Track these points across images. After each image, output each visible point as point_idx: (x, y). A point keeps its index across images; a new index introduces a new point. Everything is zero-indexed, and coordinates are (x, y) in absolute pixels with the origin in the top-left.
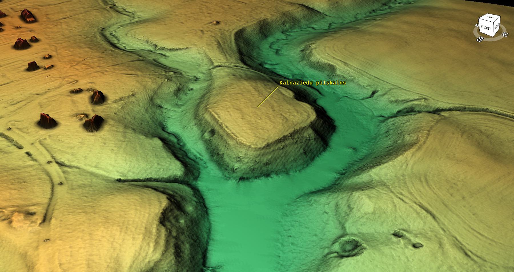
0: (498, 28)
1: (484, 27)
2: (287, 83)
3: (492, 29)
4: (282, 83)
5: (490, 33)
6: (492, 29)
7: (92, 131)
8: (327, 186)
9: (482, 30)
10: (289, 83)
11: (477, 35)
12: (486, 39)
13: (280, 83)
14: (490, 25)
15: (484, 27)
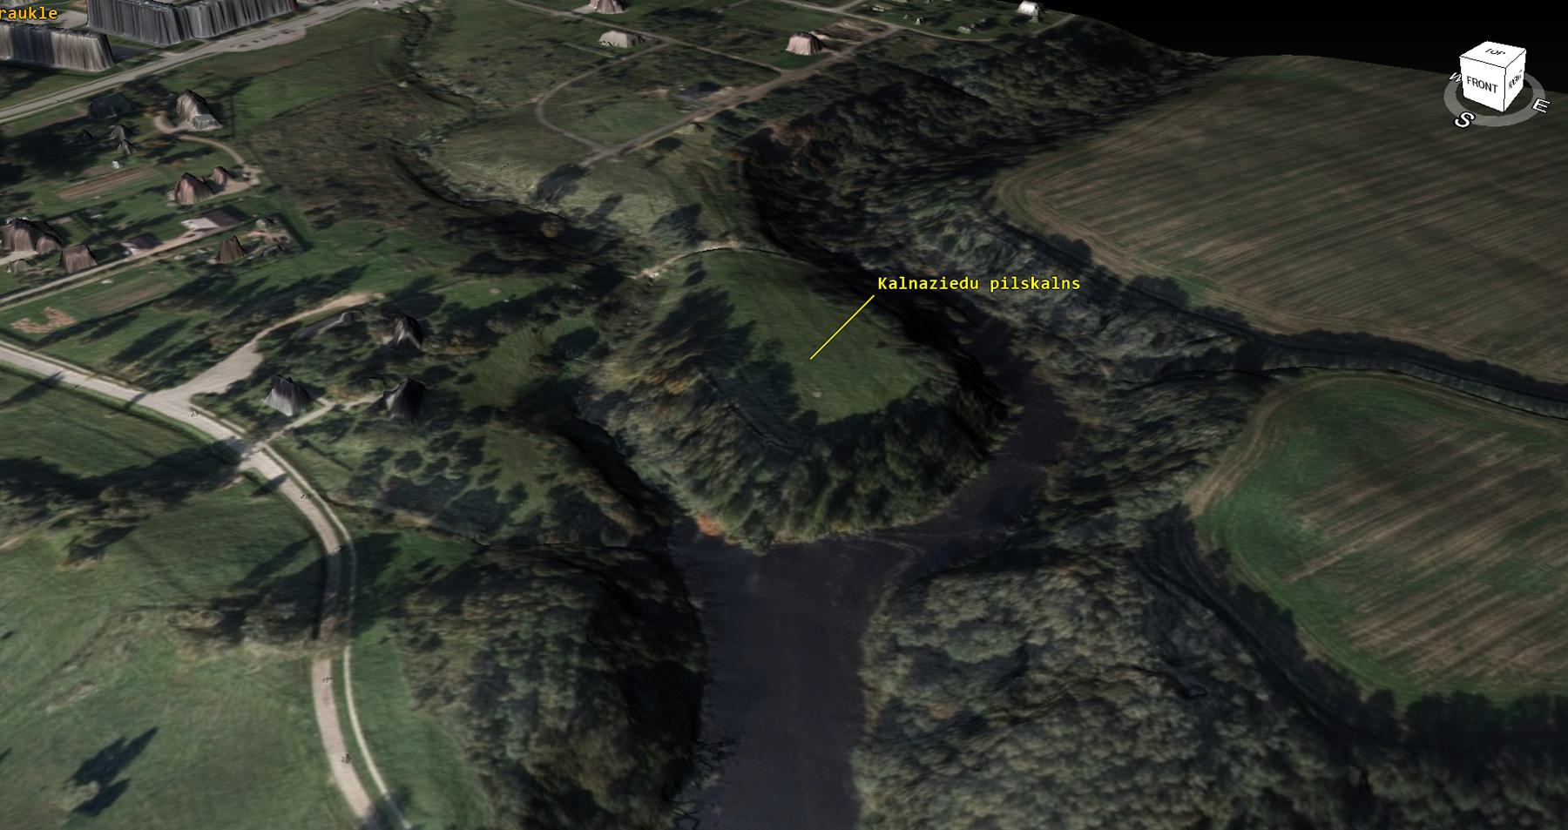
0: (1519, 86)
1: (1478, 83)
2: (899, 284)
3: (1500, 89)
4: (887, 283)
5: (1498, 101)
6: (1500, 89)
7: (1460, 697)
8: (300, 552)
9: (1471, 92)
10: (907, 284)
11: (1452, 104)
12: (1482, 121)
13: (881, 283)
14: (1494, 76)
15: (1478, 83)
